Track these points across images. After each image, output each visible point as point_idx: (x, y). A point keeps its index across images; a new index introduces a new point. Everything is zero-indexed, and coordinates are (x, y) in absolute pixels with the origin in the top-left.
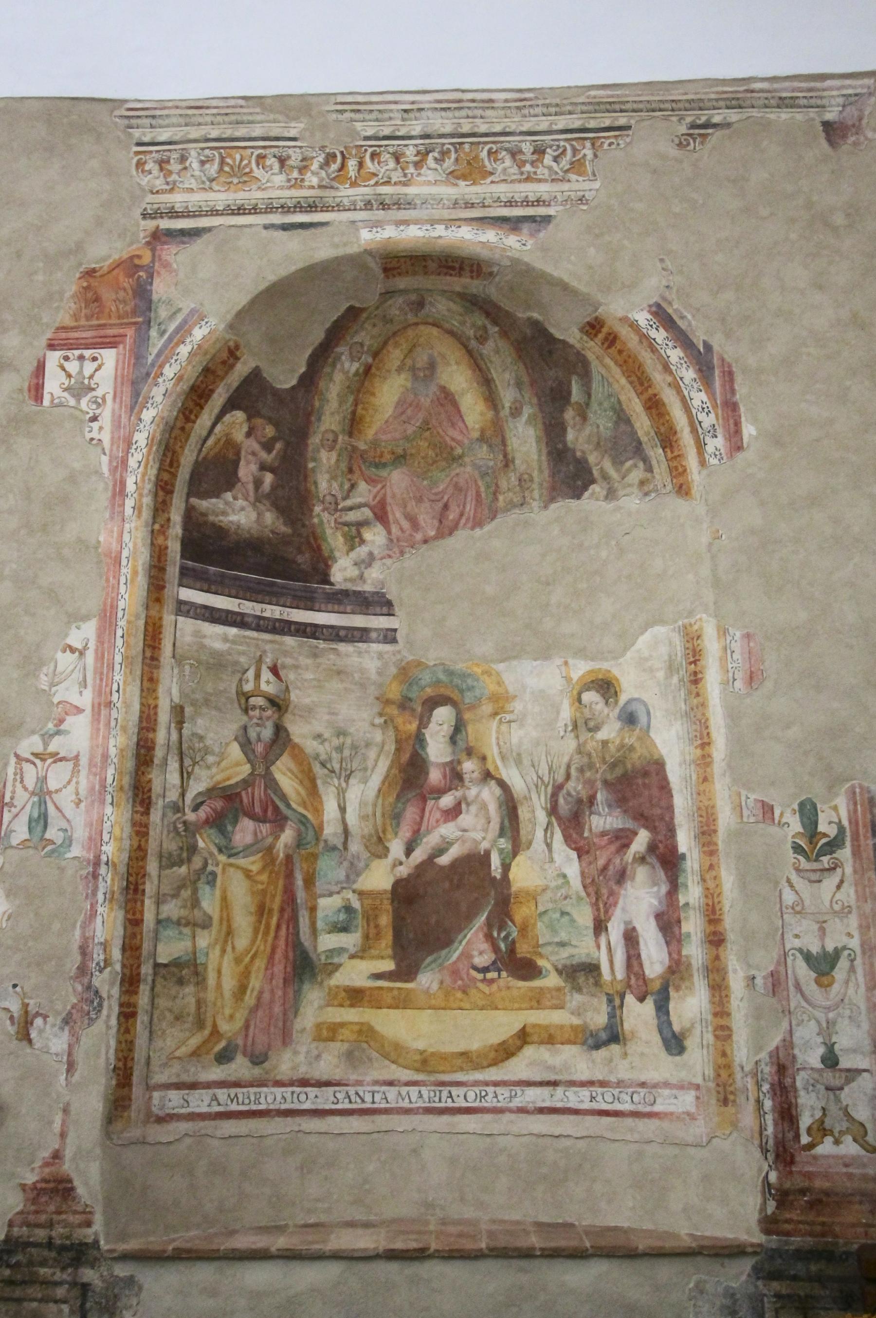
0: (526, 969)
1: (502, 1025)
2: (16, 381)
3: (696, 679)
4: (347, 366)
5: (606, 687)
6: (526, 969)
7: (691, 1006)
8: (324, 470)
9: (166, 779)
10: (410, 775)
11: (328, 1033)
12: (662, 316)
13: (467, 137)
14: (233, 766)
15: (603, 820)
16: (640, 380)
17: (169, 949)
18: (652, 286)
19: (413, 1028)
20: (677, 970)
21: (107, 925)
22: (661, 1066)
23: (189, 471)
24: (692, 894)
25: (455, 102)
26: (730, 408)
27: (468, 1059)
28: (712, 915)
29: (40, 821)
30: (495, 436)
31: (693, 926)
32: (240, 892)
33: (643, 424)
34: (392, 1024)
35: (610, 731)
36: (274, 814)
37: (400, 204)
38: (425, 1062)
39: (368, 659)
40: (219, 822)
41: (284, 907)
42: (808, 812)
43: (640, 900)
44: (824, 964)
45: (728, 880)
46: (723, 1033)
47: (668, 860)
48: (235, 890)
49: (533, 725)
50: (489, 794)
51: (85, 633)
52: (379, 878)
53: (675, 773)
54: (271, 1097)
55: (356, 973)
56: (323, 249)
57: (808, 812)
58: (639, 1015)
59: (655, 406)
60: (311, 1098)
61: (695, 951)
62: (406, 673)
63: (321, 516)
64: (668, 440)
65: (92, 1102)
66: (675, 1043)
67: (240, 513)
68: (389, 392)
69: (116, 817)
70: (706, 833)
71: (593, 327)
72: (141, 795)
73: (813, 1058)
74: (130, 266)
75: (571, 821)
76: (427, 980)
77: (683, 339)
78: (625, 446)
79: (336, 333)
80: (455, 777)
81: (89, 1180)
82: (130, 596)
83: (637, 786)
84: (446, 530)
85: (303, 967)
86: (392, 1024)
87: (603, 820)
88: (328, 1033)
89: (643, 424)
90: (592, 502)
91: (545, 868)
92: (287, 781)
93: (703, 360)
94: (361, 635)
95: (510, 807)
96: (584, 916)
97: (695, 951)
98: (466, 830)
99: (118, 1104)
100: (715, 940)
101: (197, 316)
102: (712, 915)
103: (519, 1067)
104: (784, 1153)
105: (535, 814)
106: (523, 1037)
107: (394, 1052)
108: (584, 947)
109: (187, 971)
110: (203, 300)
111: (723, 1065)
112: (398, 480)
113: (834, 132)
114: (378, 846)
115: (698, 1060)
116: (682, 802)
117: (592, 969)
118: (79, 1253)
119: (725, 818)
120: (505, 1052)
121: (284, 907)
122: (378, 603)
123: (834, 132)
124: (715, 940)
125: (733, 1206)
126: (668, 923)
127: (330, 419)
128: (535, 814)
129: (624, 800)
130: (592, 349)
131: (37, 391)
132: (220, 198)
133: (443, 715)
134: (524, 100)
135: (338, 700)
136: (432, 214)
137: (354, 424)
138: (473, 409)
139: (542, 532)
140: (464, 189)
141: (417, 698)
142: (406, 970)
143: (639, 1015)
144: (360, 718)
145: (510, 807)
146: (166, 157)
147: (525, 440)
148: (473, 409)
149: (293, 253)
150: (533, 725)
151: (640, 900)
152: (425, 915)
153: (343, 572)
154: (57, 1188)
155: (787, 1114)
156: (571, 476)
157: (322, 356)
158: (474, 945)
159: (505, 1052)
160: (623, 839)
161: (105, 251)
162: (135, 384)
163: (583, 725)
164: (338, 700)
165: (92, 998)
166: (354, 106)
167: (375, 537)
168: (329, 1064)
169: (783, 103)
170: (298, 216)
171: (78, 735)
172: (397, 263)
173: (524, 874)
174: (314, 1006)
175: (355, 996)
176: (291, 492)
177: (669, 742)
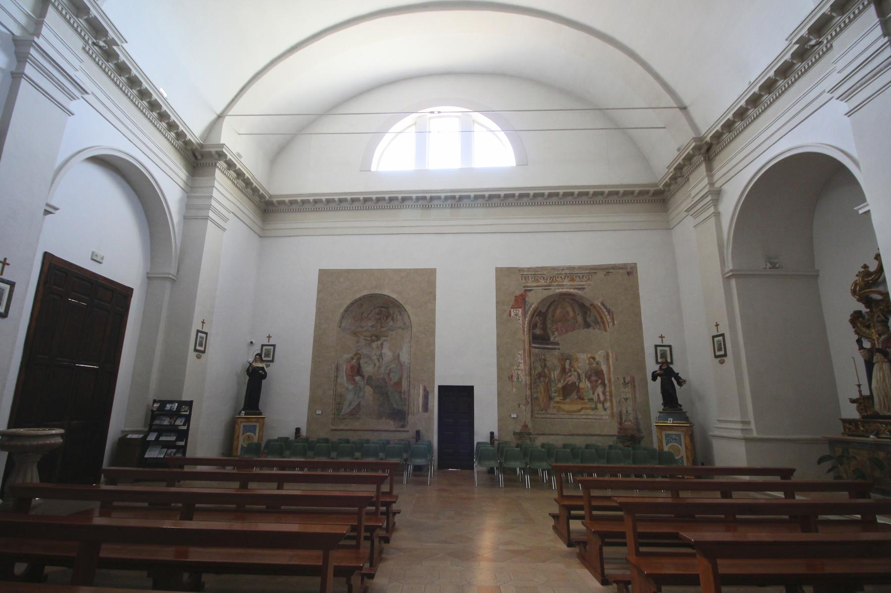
0: (583, 399)
1: (580, 407)
2: (507, 314)
3: (608, 359)
4: (553, 307)
5: (594, 358)
6: (583, 399)
7: (608, 405)
8: (549, 322)
9: (533, 372)
10: (563, 370)
11: (554, 407)
12: (603, 304)
13: (572, 273)
14: (539, 369)
15: (593, 378)
16: (599, 313)
17: (535, 396)
18: (601, 299)
19: (566, 407)
20: (605, 400)
21: (528, 392)
22: (603, 413)
23: (533, 326)
24: (608, 389)
25: (570, 268)
26: (613, 319)
27: (574, 411)
28: (611, 392)
29: (518, 378)
30: (574, 318)
31: (608, 394)
32: (542, 388)
33: (599, 320)
34: (563, 406)
35: (594, 365)
36: (545, 376)
37: (563, 285)
38: (568, 412)
39: (556, 353)
40: (539, 378)
41: (547, 390)
42: (624, 379)
43: (600, 390)
44: (626, 399)
45: (613, 388)
46: (612, 408)
47: (604, 385)
48: (541, 388)
49: (582, 361)
50: (576, 373)
51: (521, 352)
52: (560, 385)
53: (605, 372)
54: (548, 416)
55: (558, 399)
56: (551, 293)
57: (624, 379)
58: (600, 406)
59: (601, 317)
60: (553, 416)
61: (608, 397)
62: (562, 354)
63: (549, 331)
64: (603, 323)
65: (529, 415)
66: (605, 409)
67: (538, 332)
68: (559, 311)
69: (528, 378)
70: (610, 381)
71: (592, 305)
72: (530, 374)
73: (624, 412)
74: (522, 295)
75: (589, 378)
76: (568, 400)
77: (606, 308)
78: (596, 322)
79: (551, 304)
80: (570, 371)
81: (530, 425)
82: (527, 347)
83: (599, 374)
84: (567, 332)
85: (551, 398)
86: (563, 406)
87: (593, 378)
88: (554, 407)
89: (599, 320)
90: (591, 330)
91: (585, 384)
92: (547, 372)
93: (609, 311)
94: (555, 349)
95: (579, 375)
96: (591, 392)
97: (608, 397)
98: (573, 378)
99: (532, 416)
100: (611, 396)
101: (533, 304)
102: (611, 392)
103: (582, 413)
104: (621, 424)
105: (583, 377)
106: (582, 409)
107: (564, 410)
108: (591, 396)
109: (537, 398)
110: (534, 299)
111: (612, 413)
112: (560, 324)
113: (629, 273)
114: (559, 381)
115: (609, 411)
116: (606, 377)
117: (592, 399)
118: (529, 434)
119: (613, 379)
120: (580, 410)
121: (547, 390)
122: (558, 344)
123: (629, 273)
124: (611, 396)
125: (614, 429)
126: (604, 393)
127: (549, 316)
128: (583, 377)
129: (596, 375)
130: (591, 308)
131: (510, 315)
132: (535, 284)
133: (568, 361)
134: (580, 268)
135: (553, 359)
136: (567, 287)
137: (553, 316)
138: (571, 314)
139: (582, 333)
140: (572, 283)
141: (564, 358)
142: (564, 399)
143: (600, 406)
144: (556, 362)
145: (579, 375)
146: (526, 278)
147: (580, 318)
148: (571, 314)
149: (546, 293)
150: (582, 361)
151: (600, 390)
152: (568, 391)
153: (552, 339)
154: (525, 426)
155: (621, 419)
156: (587, 325)
157: (549, 307)
158: (574, 395)
159: (580, 410)
160: (597, 381)
161: (518, 293)
162: (525, 314)
163: (590, 364)
164: (553, 359)
165: (528, 402)
166: (554, 269)
167: (556, 333)
168: (555, 411)
169: (622, 268)
170: (546, 287)
171: (522, 366)
172: (561, 294)
173: (582, 385)
174: (552, 404)
175: (558, 402)
176: (544, 328)
177: (604, 368)
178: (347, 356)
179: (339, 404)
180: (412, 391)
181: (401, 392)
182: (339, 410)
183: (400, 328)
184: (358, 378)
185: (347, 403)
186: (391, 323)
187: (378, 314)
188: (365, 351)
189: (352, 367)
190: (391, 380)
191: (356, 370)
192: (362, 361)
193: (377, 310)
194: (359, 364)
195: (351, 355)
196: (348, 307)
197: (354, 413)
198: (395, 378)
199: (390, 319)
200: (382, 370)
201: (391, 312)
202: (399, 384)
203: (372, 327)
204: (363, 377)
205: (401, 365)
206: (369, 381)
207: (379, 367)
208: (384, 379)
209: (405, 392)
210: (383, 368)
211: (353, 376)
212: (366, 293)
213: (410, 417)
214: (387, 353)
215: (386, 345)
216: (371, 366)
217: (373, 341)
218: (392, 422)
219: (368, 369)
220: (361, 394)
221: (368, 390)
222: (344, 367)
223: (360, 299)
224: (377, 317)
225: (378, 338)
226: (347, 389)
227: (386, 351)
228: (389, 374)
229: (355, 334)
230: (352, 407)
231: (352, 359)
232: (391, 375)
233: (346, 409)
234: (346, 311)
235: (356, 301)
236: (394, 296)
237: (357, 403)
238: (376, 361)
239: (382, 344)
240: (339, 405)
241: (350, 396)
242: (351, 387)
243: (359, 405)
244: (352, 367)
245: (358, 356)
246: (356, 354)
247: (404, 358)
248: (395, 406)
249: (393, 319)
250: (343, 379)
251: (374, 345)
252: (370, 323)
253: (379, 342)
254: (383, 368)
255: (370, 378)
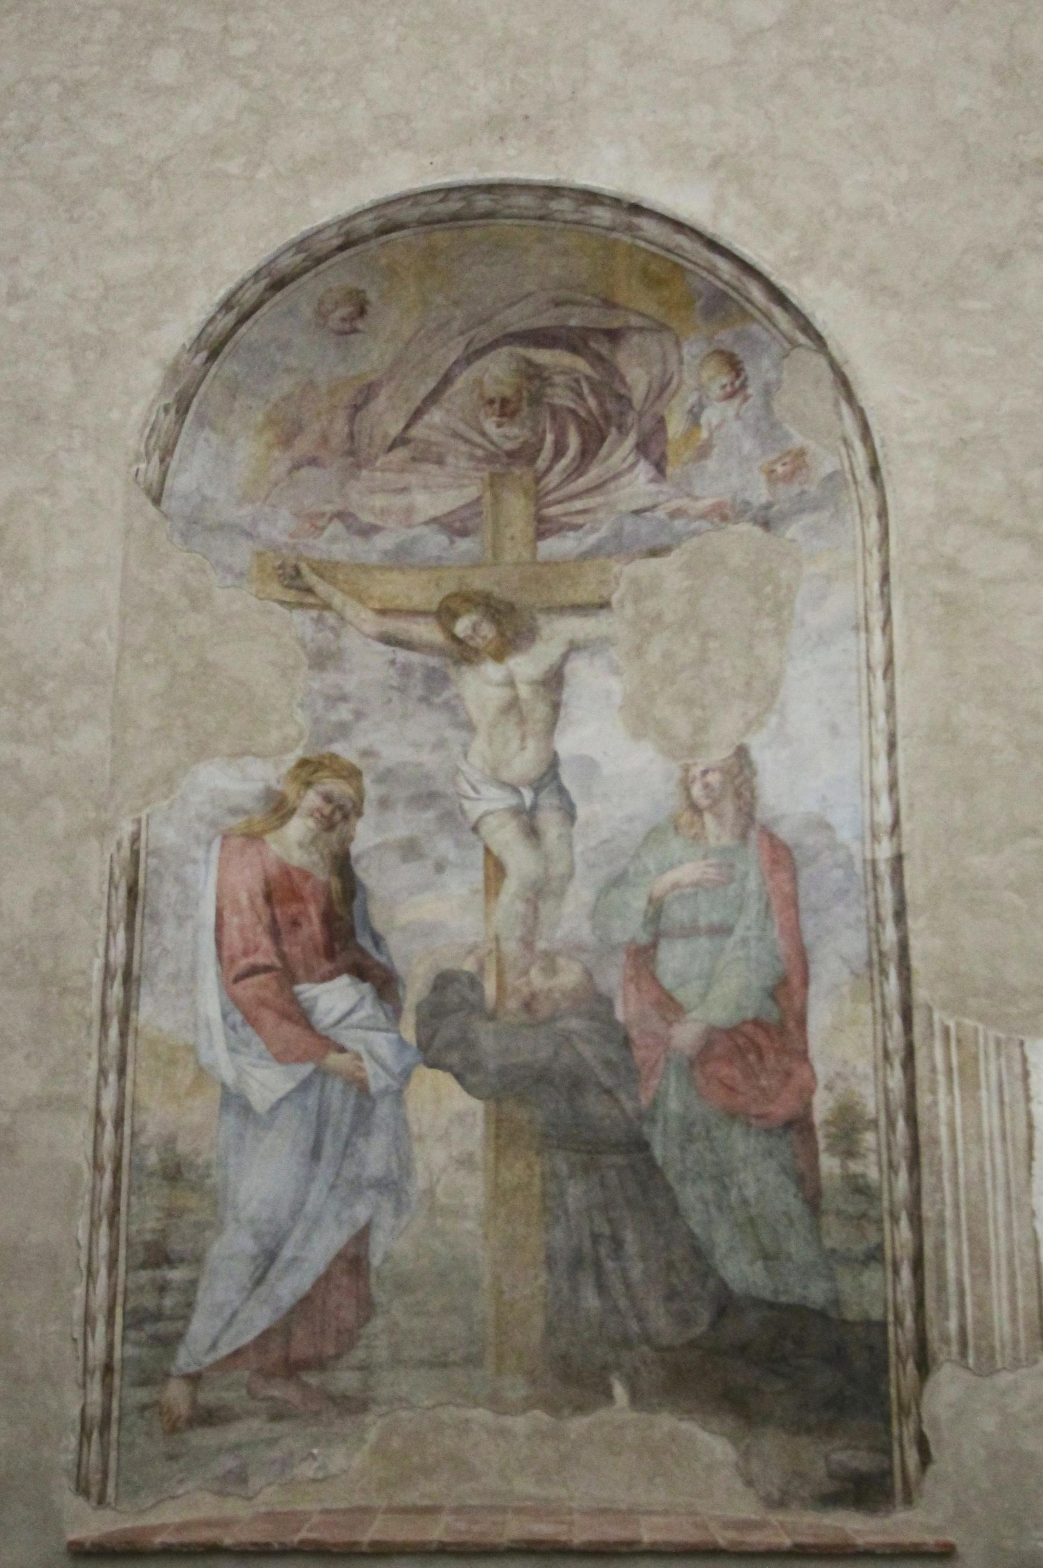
178: (234, 781)
179: (158, 1256)
180: (941, 1105)
181: (800, 1124)
182: (156, 1325)
183: (723, 514)
184: (334, 998)
185: (231, 1249)
186: (639, 483)
187: (505, 409)
188: (392, 741)
189: (280, 891)
190: (669, 1007)
191: (324, 923)
192: (365, 836)
193: (497, 371)
194: (343, 865)
195: (265, 774)
196: (239, 310)
197: (310, 1355)
198: (715, 986)
199: (620, 451)
200: (571, 918)
201: (638, 379)
202: (771, 1034)
203: (455, 526)
204: (384, 984)
205: (781, 856)
206: (449, 1023)
207: (540, 892)
208: (595, 1004)
209: (849, 1124)
210: (580, 896)
211: (288, 975)
212: (399, 175)
213: (947, 1389)
214: (617, 756)
215: (596, 690)
216: (464, 882)
217: (464, 653)
218: (712, 1444)
219: (431, 913)
220: (375, 1154)
221: (445, 1116)
222: (203, 894)
223: (349, 238)
224: (506, 435)
225: (510, 625)
226: (234, 1101)
227: (596, 732)
228: (643, 957)
229: (295, 581)
230: (289, 1287)
231: (279, 809)
232: (673, 960)
233: (226, 1313)
234: (213, 347)
235: (311, 255)
236: (690, 203)
237: (319, 1249)
238: (505, 837)
239: (554, 681)
240: (157, 1265)
241: (261, 1179)
242: (268, 1082)
243: (353, 1261)
244: (280, 891)
245: (331, 786)
246: (309, 769)
247: (815, 774)
248: (740, 1270)
249: (652, 448)
250: (192, 1004)
251: (481, 687)
252: (435, 496)
253: (525, 667)
254: (580, 896)
255: (452, 997)
